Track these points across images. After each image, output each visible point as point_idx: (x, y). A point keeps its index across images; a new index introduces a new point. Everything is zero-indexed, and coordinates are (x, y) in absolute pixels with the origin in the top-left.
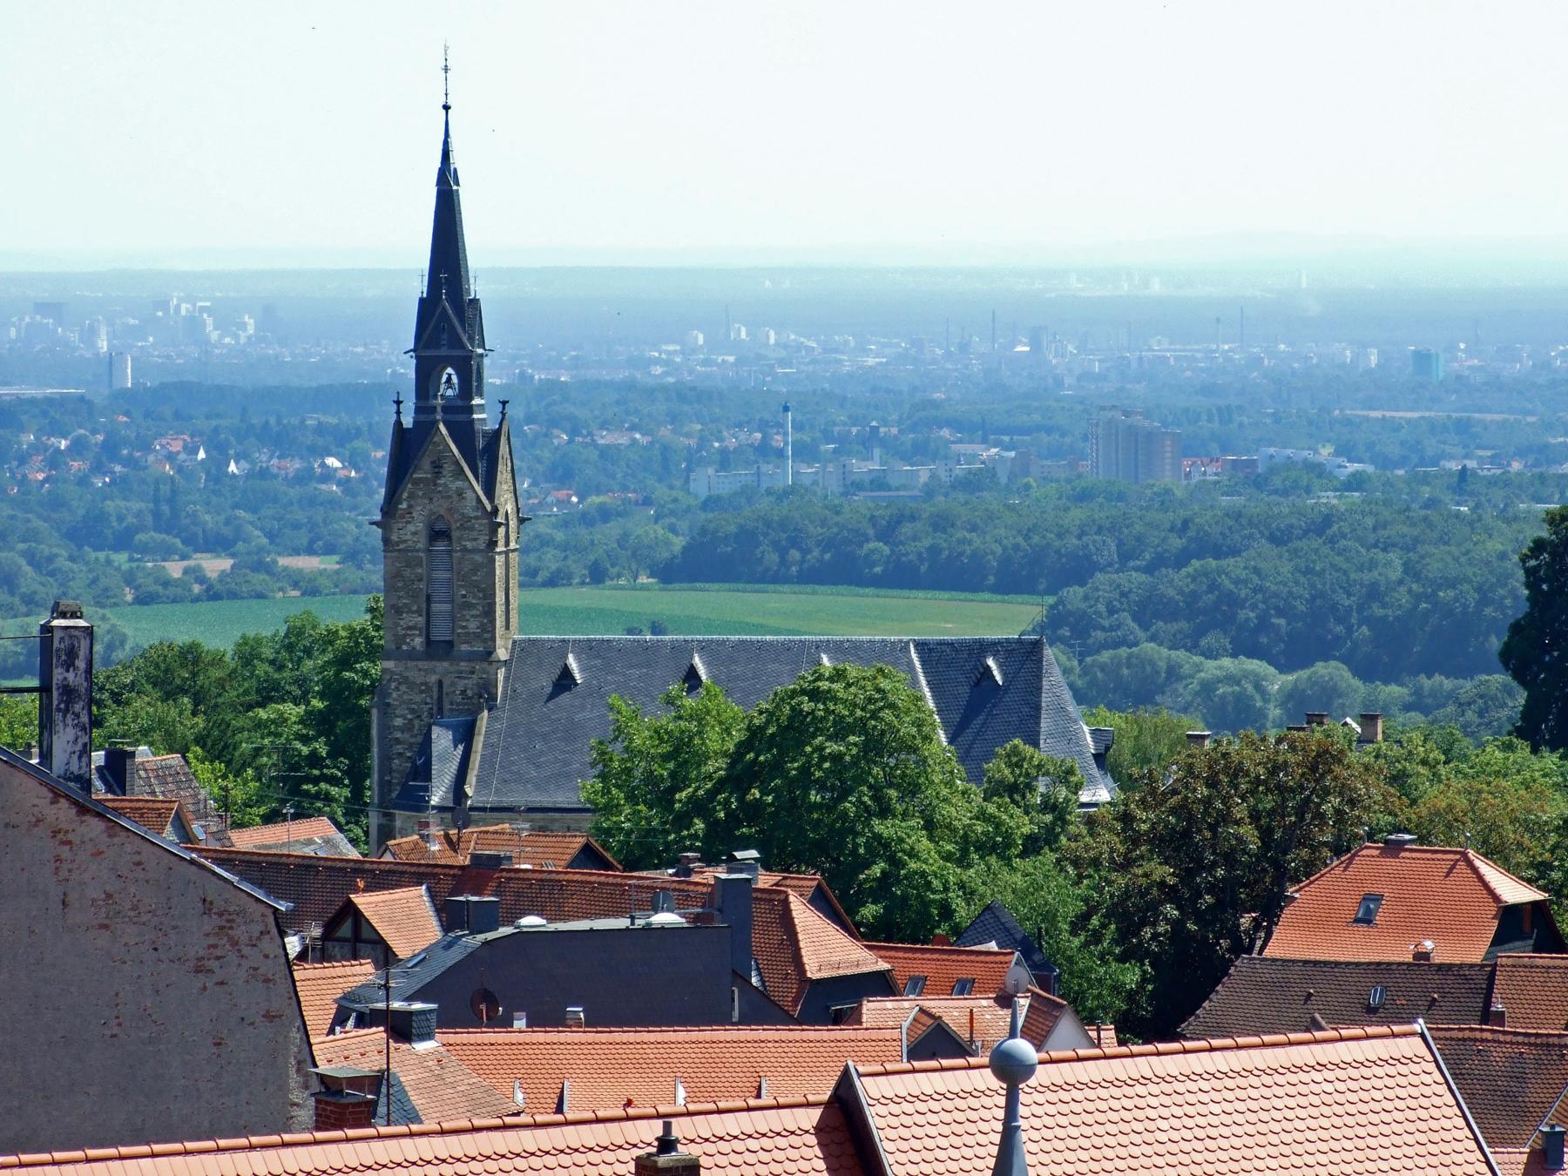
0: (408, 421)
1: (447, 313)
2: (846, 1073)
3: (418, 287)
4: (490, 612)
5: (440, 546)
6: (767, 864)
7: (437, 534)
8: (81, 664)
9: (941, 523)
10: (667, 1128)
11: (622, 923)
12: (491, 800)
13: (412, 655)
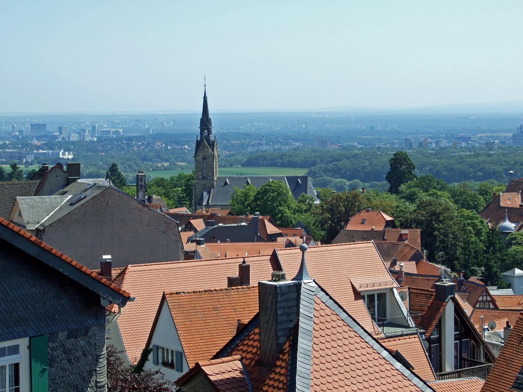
0: (199, 139)
1: (205, 121)
2: (274, 251)
3: (201, 116)
4: (213, 172)
5: (204, 161)
6: (261, 214)
7: (204, 159)
8: (143, 181)
9: (290, 156)
10: (244, 259)
11: (236, 225)
12: (214, 204)
13: (200, 179)
